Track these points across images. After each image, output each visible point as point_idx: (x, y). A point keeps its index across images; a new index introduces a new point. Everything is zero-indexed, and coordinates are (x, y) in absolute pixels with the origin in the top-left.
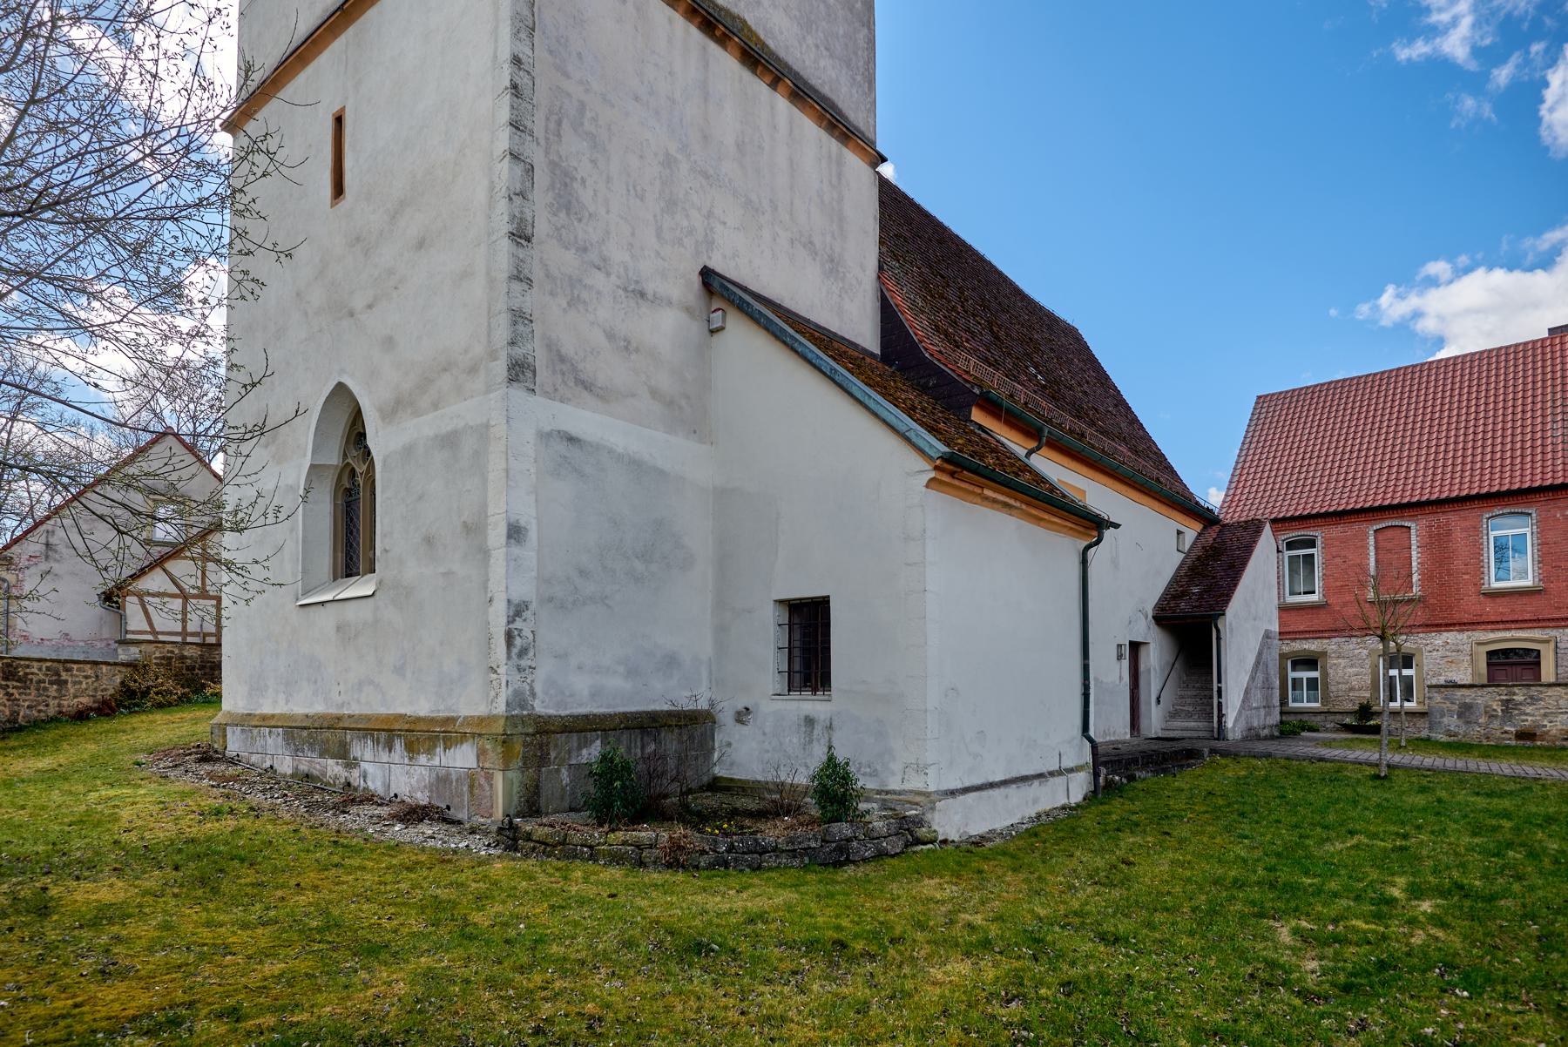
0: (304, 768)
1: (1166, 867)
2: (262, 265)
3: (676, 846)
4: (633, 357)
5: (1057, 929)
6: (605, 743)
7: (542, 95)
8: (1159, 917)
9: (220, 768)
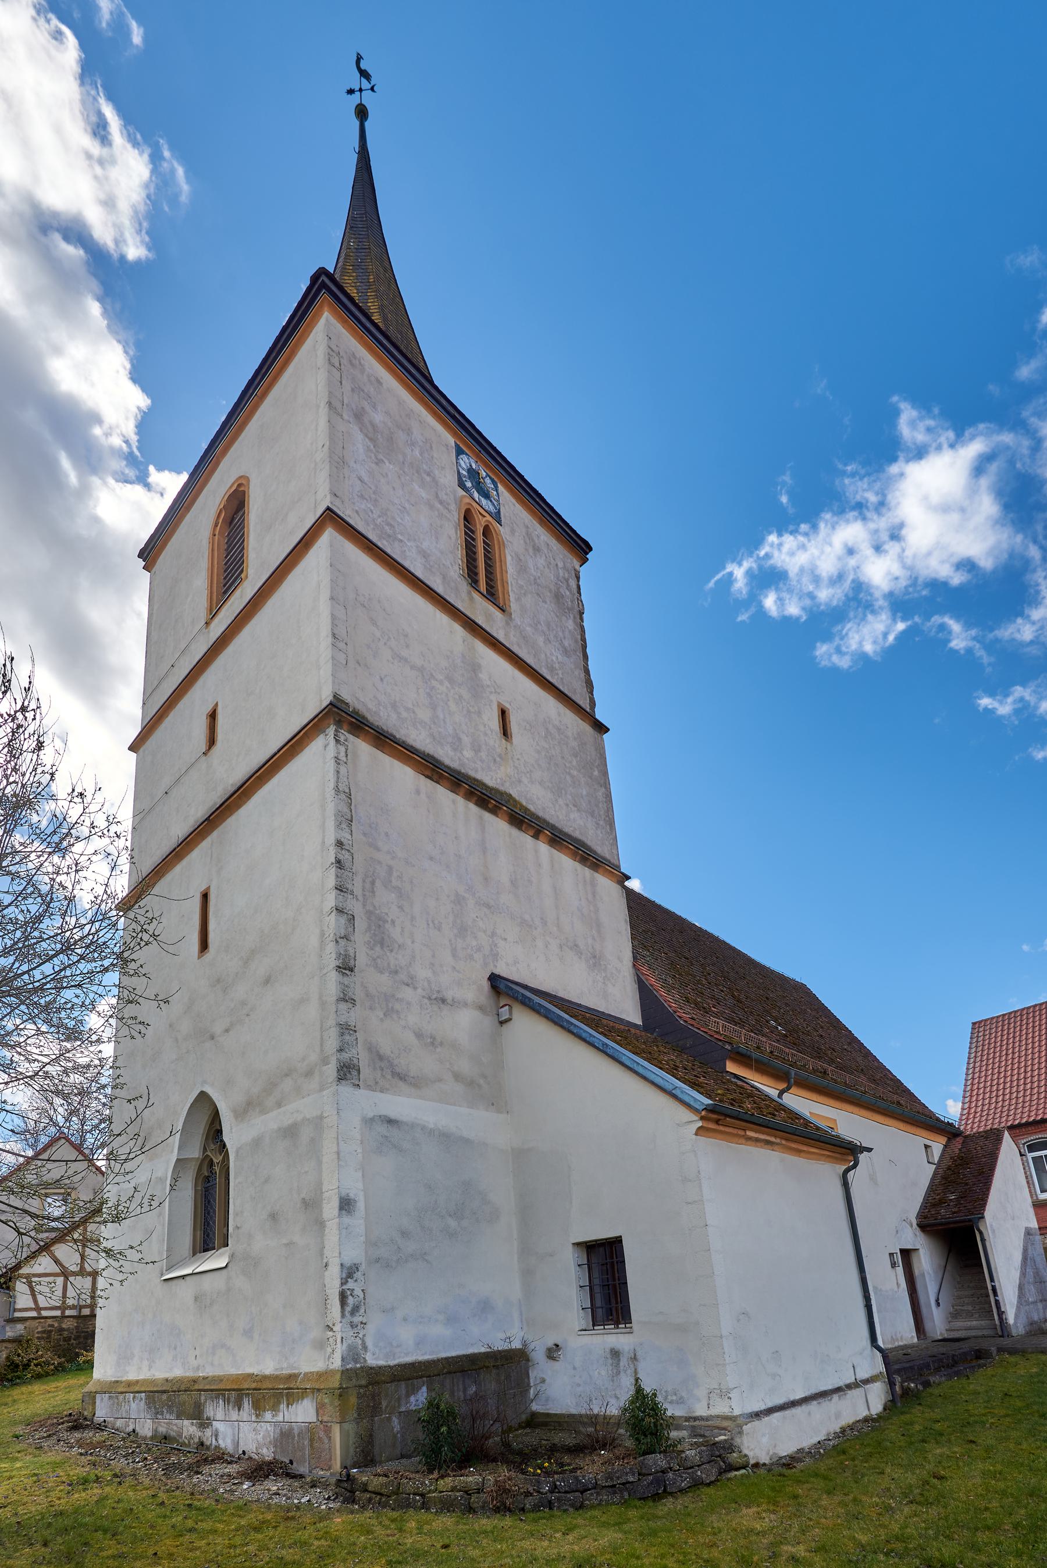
0: (162, 1430)
1: (978, 1481)
2: (146, 1010)
3: (503, 1490)
4: (439, 1050)
5: (882, 1557)
6: (430, 1390)
7: (359, 866)
8: (982, 1537)
9: (88, 1434)
